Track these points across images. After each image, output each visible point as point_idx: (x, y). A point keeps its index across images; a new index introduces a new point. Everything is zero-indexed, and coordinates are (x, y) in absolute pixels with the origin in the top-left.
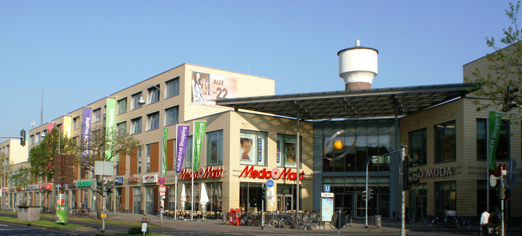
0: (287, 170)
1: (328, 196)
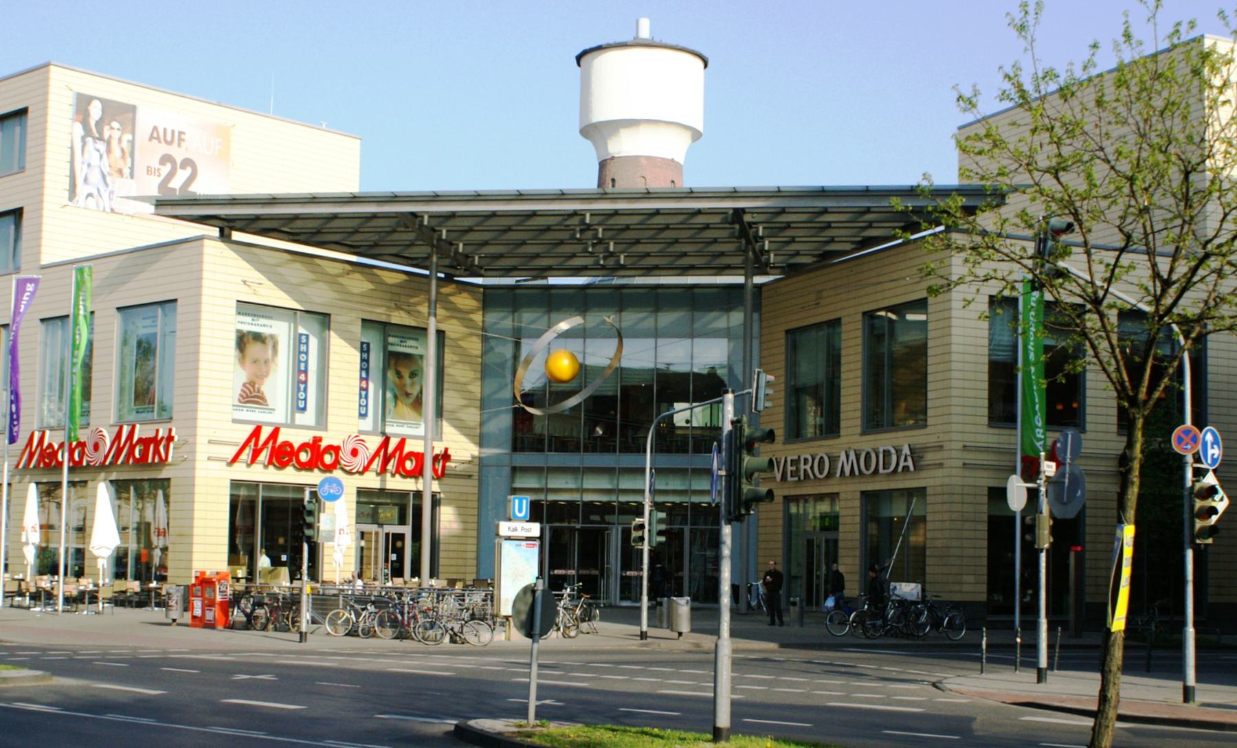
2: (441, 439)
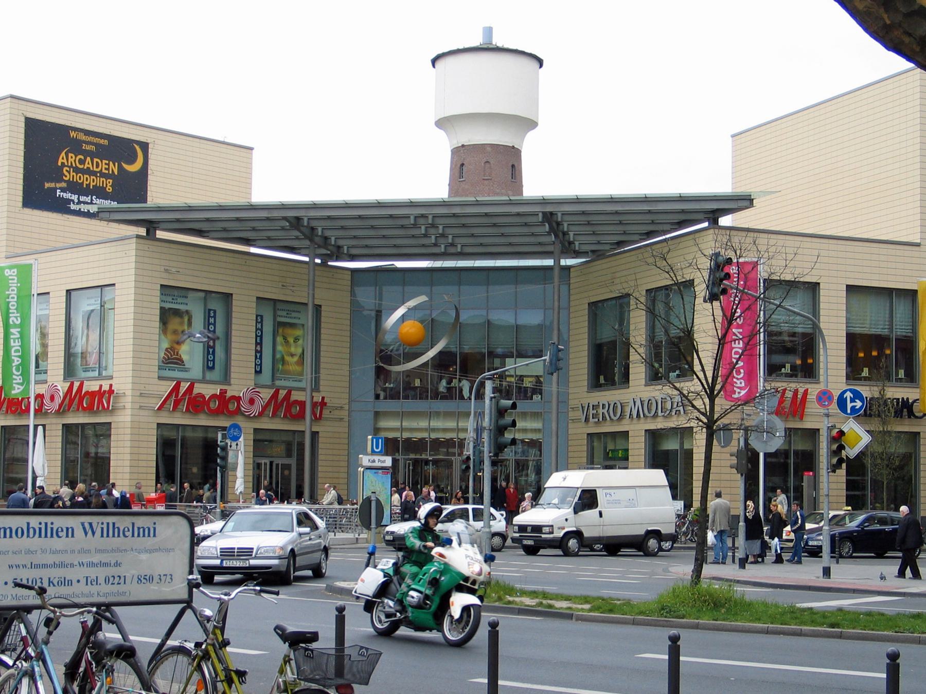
0: (282, 393)
1: (377, 464)
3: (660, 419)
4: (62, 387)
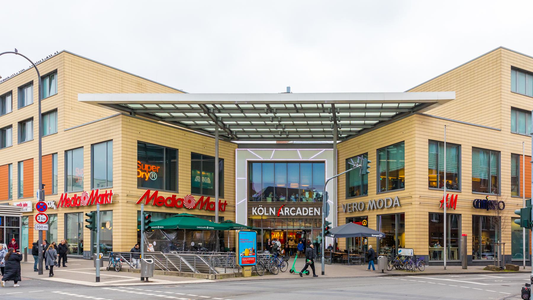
2: (223, 198)
3: (384, 210)
4: (89, 193)
